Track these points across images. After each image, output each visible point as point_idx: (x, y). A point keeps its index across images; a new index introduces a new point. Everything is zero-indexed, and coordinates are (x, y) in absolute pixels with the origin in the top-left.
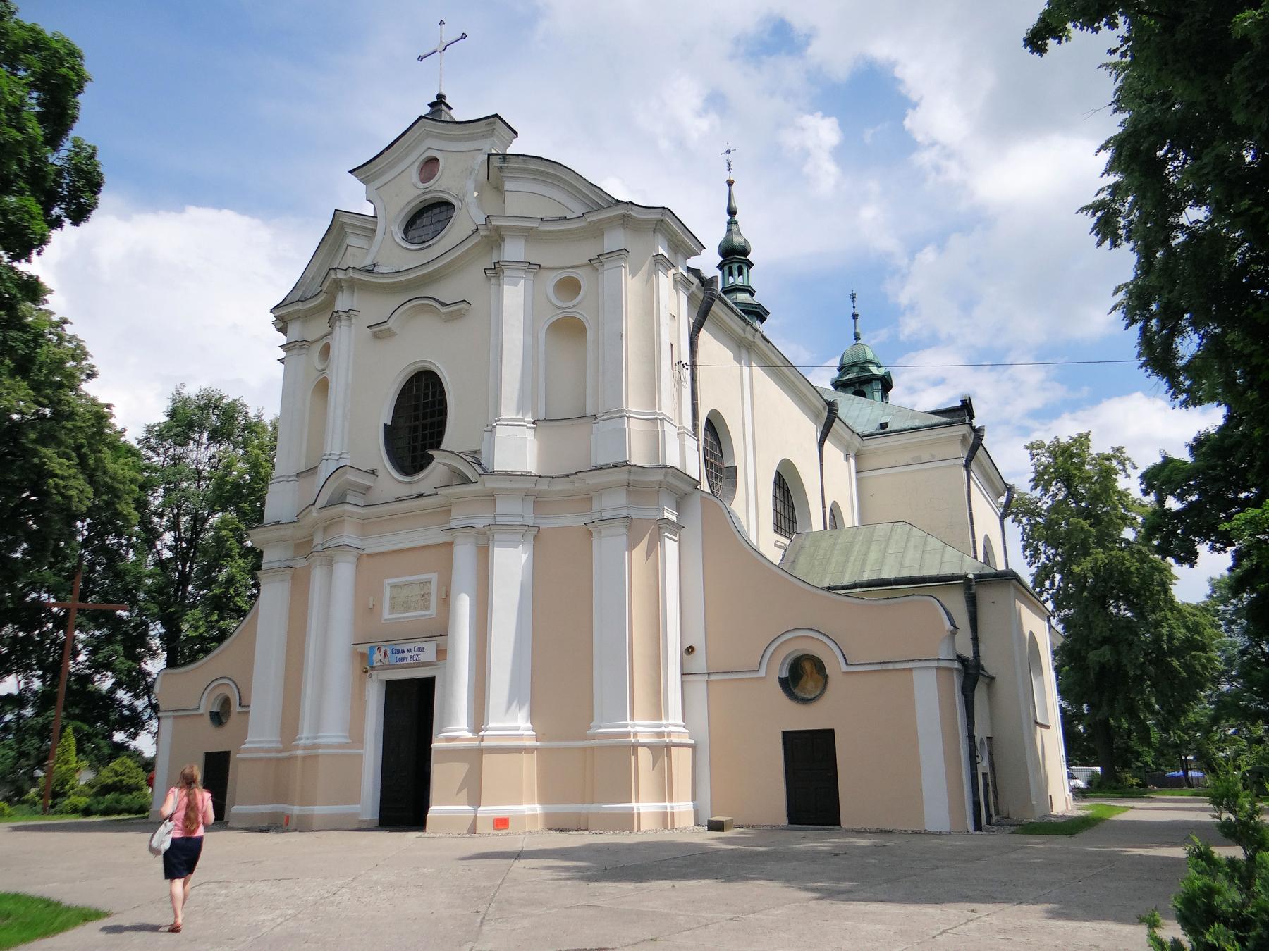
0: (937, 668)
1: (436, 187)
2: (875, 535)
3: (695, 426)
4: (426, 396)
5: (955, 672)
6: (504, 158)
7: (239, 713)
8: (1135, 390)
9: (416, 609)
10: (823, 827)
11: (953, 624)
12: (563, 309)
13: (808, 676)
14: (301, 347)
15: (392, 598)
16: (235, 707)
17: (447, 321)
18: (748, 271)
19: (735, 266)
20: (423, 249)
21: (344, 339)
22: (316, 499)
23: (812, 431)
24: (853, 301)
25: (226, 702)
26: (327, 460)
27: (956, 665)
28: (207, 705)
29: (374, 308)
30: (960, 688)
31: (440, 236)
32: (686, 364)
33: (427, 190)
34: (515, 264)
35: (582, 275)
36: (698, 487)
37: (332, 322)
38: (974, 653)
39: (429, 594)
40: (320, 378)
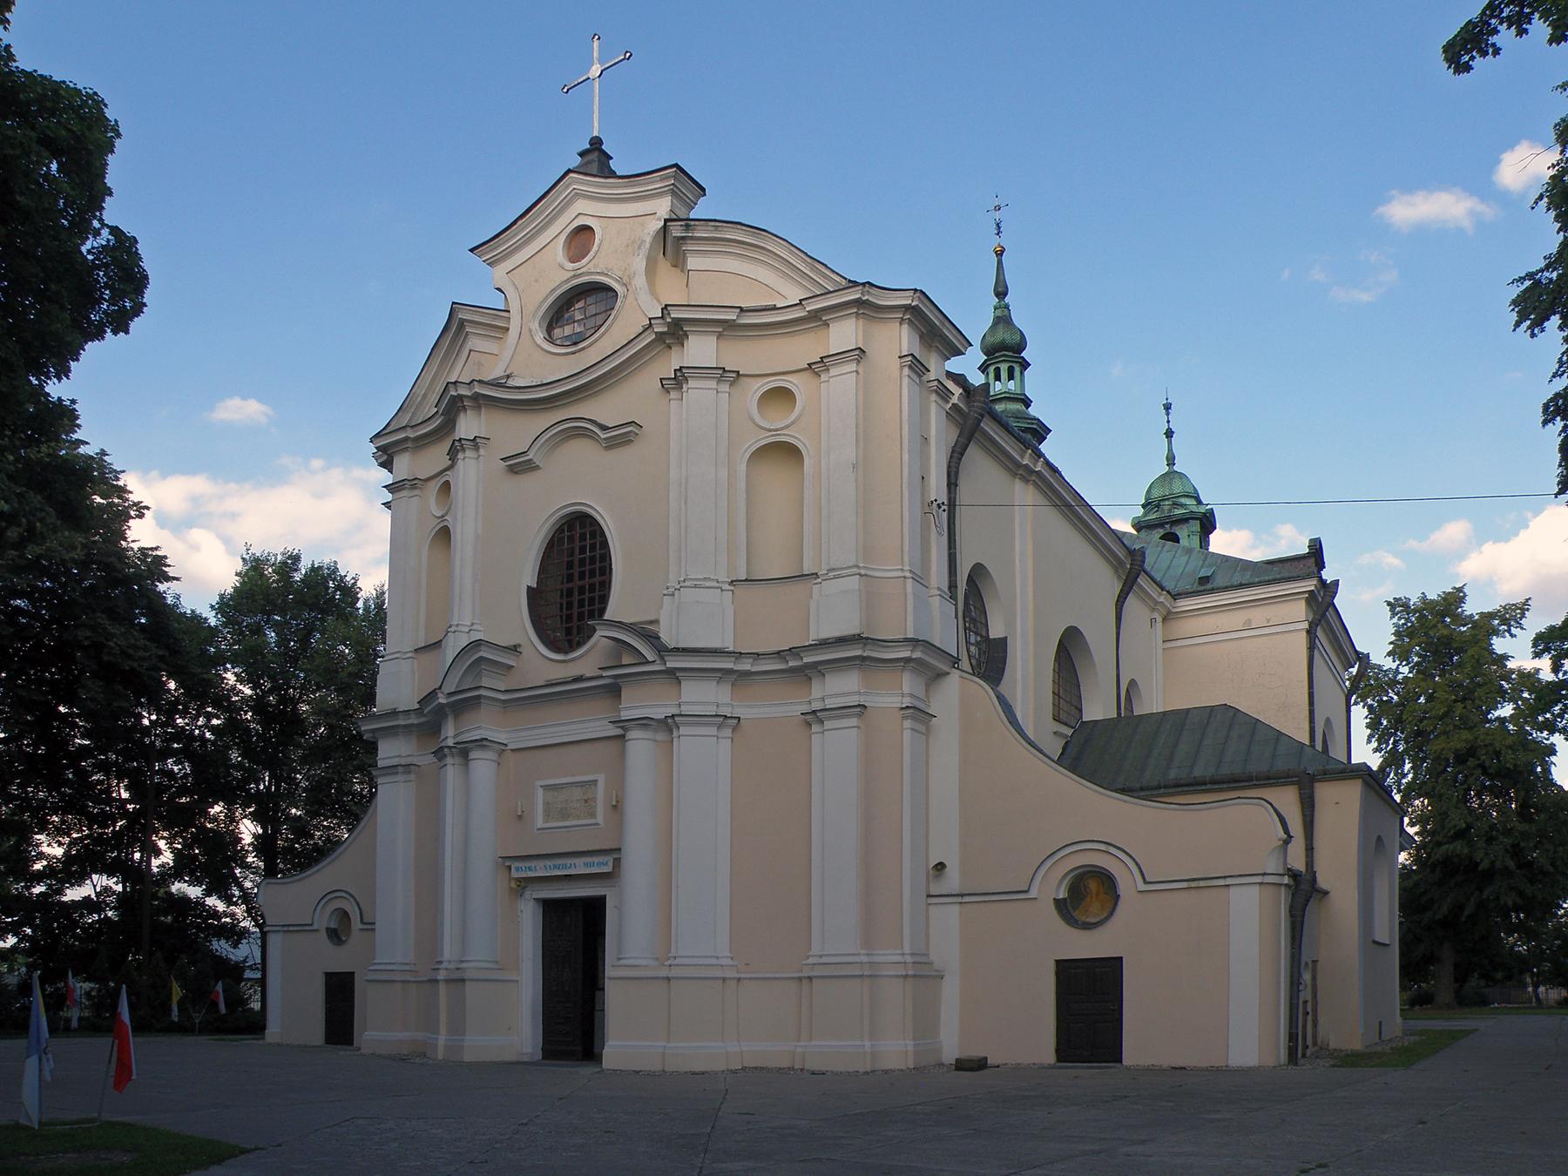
0: (1261, 884)
3: (953, 586)
4: (583, 550)
5: (1283, 888)
7: (361, 930)
8: (1519, 531)
10: (1090, 1065)
11: (1286, 830)
12: (770, 430)
13: (1092, 897)
14: (414, 487)
15: (547, 804)
16: (356, 924)
17: (608, 448)
18: (1022, 373)
19: (1004, 367)
20: (573, 353)
21: (470, 473)
22: (442, 683)
23: (1111, 586)
24: (1168, 414)
25: (344, 915)
26: (455, 632)
27: (1286, 880)
28: (324, 920)
29: (515, 433)
31: (602, 330)
32: (943, 503)
33: (579, 272)
34: (702, 371)
36: (956, 666)
37: (453, 453)
38: (1307, 865)
39: (594, 800)
40: (438, 528)
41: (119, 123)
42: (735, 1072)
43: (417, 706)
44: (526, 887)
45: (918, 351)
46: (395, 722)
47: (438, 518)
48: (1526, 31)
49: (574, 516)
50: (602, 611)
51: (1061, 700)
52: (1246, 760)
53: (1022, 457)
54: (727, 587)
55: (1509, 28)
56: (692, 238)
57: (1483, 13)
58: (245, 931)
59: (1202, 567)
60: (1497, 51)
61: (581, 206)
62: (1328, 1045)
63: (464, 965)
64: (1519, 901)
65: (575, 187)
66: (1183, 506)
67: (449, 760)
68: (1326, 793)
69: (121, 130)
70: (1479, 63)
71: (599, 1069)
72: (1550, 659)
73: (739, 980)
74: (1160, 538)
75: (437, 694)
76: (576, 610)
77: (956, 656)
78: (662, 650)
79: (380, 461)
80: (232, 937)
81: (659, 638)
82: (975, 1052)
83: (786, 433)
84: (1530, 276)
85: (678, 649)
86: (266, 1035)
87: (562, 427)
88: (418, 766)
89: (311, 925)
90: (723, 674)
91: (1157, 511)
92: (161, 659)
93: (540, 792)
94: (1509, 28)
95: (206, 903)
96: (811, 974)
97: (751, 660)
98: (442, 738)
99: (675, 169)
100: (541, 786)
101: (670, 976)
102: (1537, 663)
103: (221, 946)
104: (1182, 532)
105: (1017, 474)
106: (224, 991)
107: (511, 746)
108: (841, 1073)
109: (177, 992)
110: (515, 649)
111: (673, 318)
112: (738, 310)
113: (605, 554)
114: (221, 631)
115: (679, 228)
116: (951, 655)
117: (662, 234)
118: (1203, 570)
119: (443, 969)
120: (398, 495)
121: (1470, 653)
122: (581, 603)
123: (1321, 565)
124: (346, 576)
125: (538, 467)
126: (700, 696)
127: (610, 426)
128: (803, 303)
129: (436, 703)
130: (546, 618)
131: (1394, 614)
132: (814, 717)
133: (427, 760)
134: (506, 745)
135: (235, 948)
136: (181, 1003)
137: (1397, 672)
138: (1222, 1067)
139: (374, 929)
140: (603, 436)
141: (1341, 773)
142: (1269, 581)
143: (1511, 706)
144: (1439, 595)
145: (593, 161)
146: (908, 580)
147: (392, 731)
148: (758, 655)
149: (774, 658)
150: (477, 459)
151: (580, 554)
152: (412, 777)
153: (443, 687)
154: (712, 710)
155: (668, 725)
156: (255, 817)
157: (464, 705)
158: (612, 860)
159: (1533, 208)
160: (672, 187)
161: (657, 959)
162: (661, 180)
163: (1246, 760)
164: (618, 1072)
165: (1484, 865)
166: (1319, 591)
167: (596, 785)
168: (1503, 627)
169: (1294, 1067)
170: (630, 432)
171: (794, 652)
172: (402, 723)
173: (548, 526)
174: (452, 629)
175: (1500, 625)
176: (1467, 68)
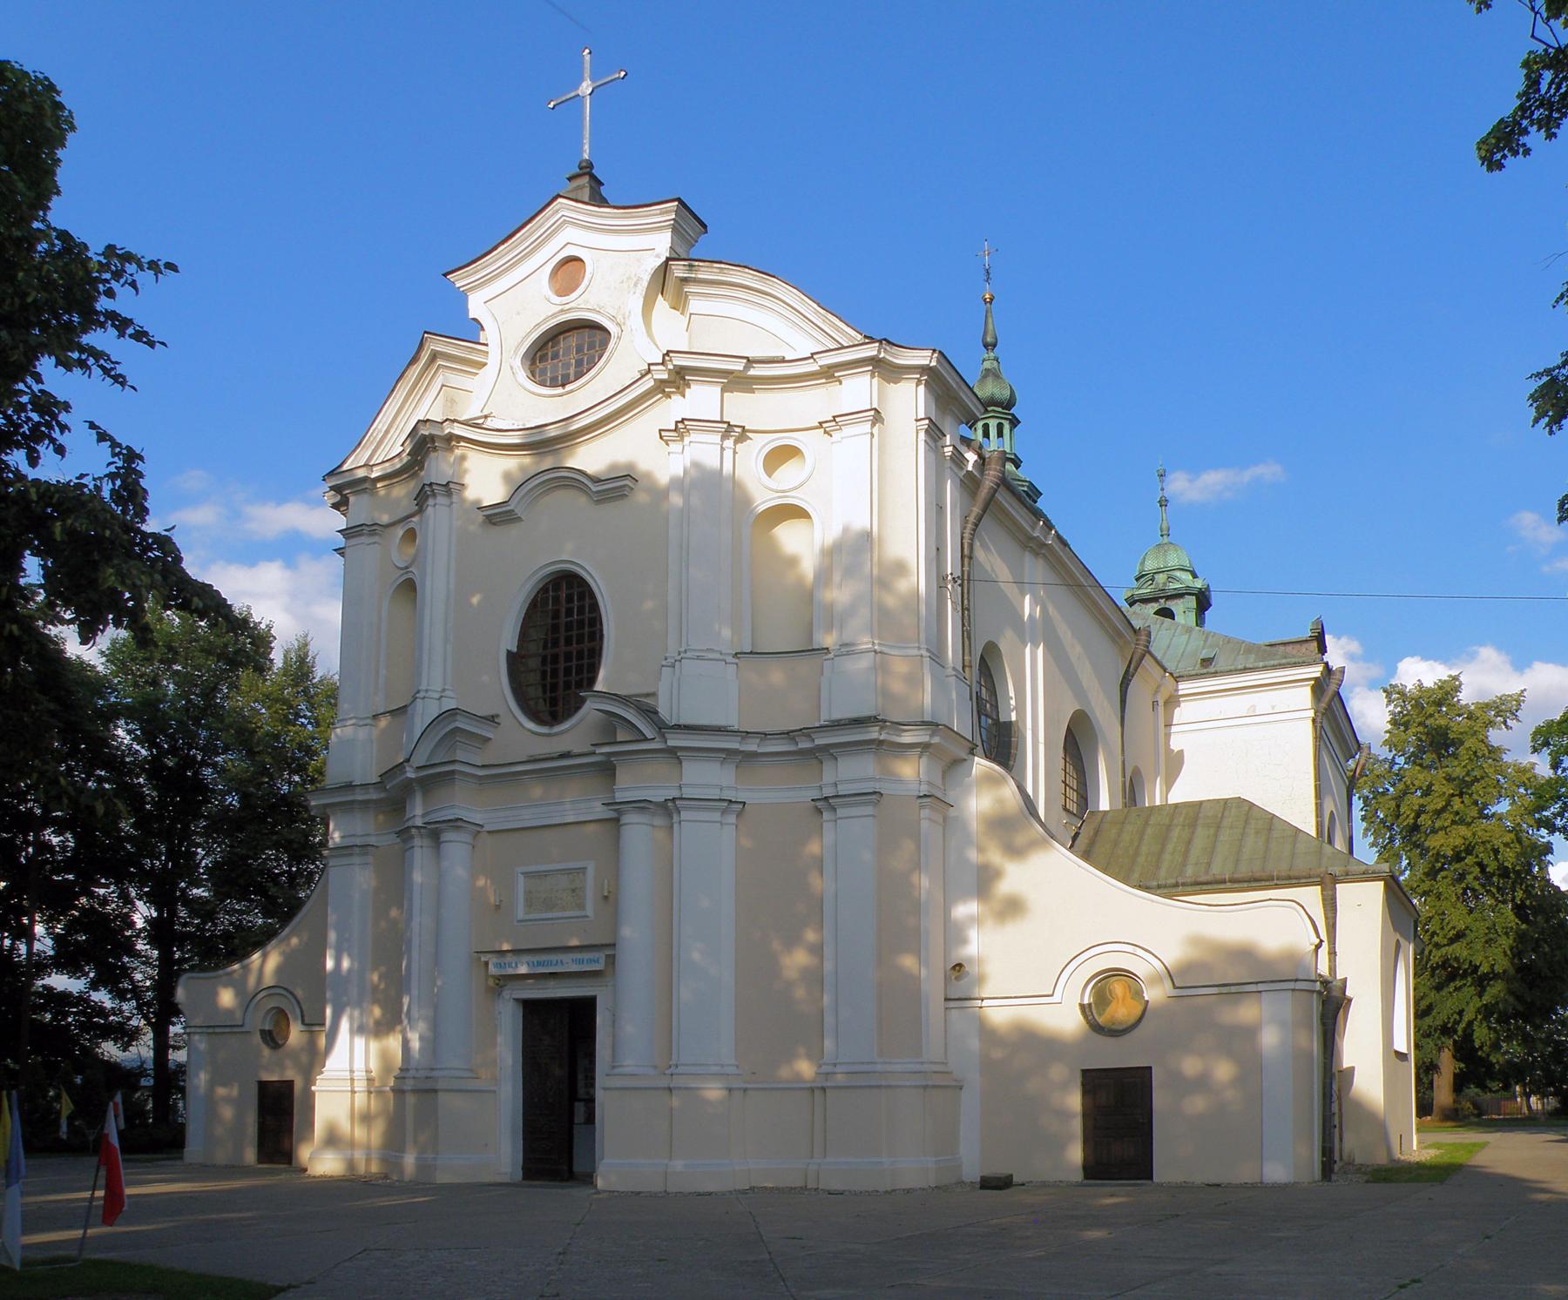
1: (581, 303)
2: (1201, 815)
4: (569, 612)
5: (1315, 995)
13: (1118, 1002)
14: (372, 533)
15: (528, 893)
17: (598, 502)
19: (993, 424)
26: (424, 698)
30: (1319, 1015)
33: (567, 307)
35: (808, 443)
38: (1330, 969)
41: (74, 115)
42: (744, 1192)
43: (379, 780)
44: (505, 985)
45: (934, 414)
46: (349, 798)
47: (402, 569)
48: (1555, 135)
49: (555, 576)
50: (592, 681)
51: (1068, 788)
52: (1265, 857)
53: (1033, 529)
54: (730, 659)
55: (1538, 130)
57: (1515, 112)
58: (137, 1030)
59: (1203, 648)
60: (1527, 152)
61: (569, 234)
62: (1354, 1160)
63: (435, 1074)
64: (1520, 1008)
65: (563, 213)
66: (1178, 580)
67: (417, 842)
68: (1346, 892)
69: (75, 123)
70: (1510, 161)
71: (593, 1191)
72: (1549, 754)
73: (745, 1090)
74: (1154, 613)
75: (404, 768)
76: (561, 678)
77: (971, 739)
78: (662, 727)
80: (122, 1039)
81: (656, 713)
82: (998, 1169)
83: (794, 495)
84: (1548, 372)
85: (679, 726)
86: (185, 1154)
87: (546, 478)
88: (377, 847)
89: (242, 1026)
90: (727, 755)
91: (1152, 584)
92: (52, 714)
94: (1538, 130)
95: (92, 998)
96: (825, 1084)
97: (758, 740)
98: (407, 817)
99: (676, 203)
100: (522, 873)
101: (671, 1086)
102: (1534, 758)
103: (110, 1049)
104: (1177, 606)
105: (1027, 547)
106: (123, 1103)
107: (487, 828)
108: (861, 1192)
109: (66, 1107)
110: (492, 719)
111: (675, 366)
112: (745, 361)
113: (595, 618)
114: (110, 682)
115: (682, 267)
116: (965, 738)
117: (663, 270)
118: (1204, 652)
119: (409, 1078)
120: (353, 541)
121: (1467, 745)
122: (568, 671)
123: (1323, 649)
124: (261, 623)
125: (519, 519)
126: (703, 777)
127: (603, 479)
128: (815, 357)
129: (404, 777)
130: (528, 686)
131: (1390, 702)
132: (825, 804)
133: (388, 840)
134: (482, 826)
135: (124, 1051)
136: (71, 1118)
137: (1393, 762)
138: (1256, 1183)
140: (594, 489)
141: (1364, 874)
142: (1274, 666)
143: (1507, 802)
144: (1435, 683)
145: (583, 187)
146: (924, 659)
147: (348, 807)
148: (766, 734)
149: (783, 738)
150: (449, 506)
151: (567, 616)
152: (370, 859)
153: (412, 759)
154: (715, 794)
155: (668, 809)
156: (151, 899)
157: (435, 780)
158: (604, 958)
159: (1554, 307)
160: (672, 222)
161: (655, 1067)
162: (660, 214)
163: (1265, 857)
164: (616, 1194)
165: (1484, 969)
166: (1324, 679)
167: (584, 874)
168: (1499, 718)
169: (1330, 1183)
170: (625, 486)
171: (806, 732)
172: (360, 798)
173: (528, 587)
174: (421, 695)
175: (1496, 716)
176: (1500, 166)
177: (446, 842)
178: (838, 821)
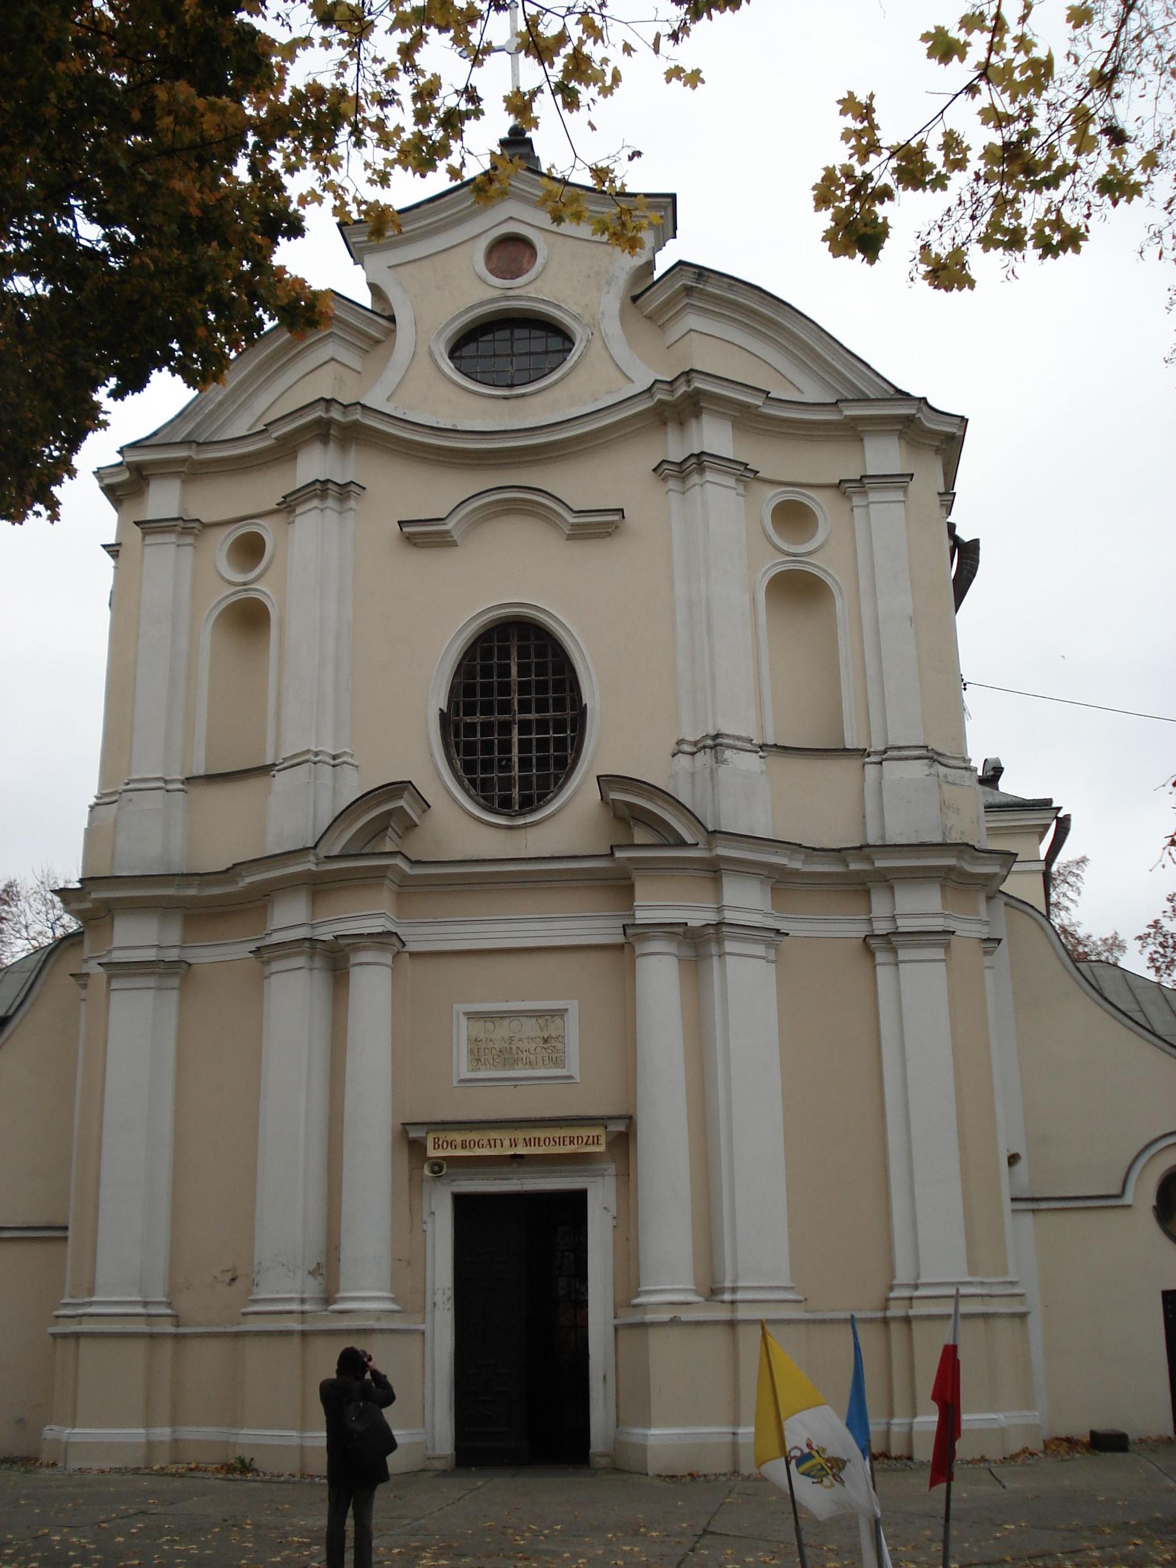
1: (531, 291)
6: (700, 275)
9: (531, 1064)
14: (186, 531)
15: (474, 1041)
17: (570, 537)
20: (506, 398)
33: (510, 293)
35: (822, 504)
39: (561, 1038)
56: (701, 291)
73: (304, 1334)
79: (108, 481)
93: (463, 1020)
139: (66, 1239)
153: (319, 846)
167: (562, 1017)
177: (361, 964)
178: (900, 965)
